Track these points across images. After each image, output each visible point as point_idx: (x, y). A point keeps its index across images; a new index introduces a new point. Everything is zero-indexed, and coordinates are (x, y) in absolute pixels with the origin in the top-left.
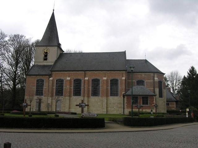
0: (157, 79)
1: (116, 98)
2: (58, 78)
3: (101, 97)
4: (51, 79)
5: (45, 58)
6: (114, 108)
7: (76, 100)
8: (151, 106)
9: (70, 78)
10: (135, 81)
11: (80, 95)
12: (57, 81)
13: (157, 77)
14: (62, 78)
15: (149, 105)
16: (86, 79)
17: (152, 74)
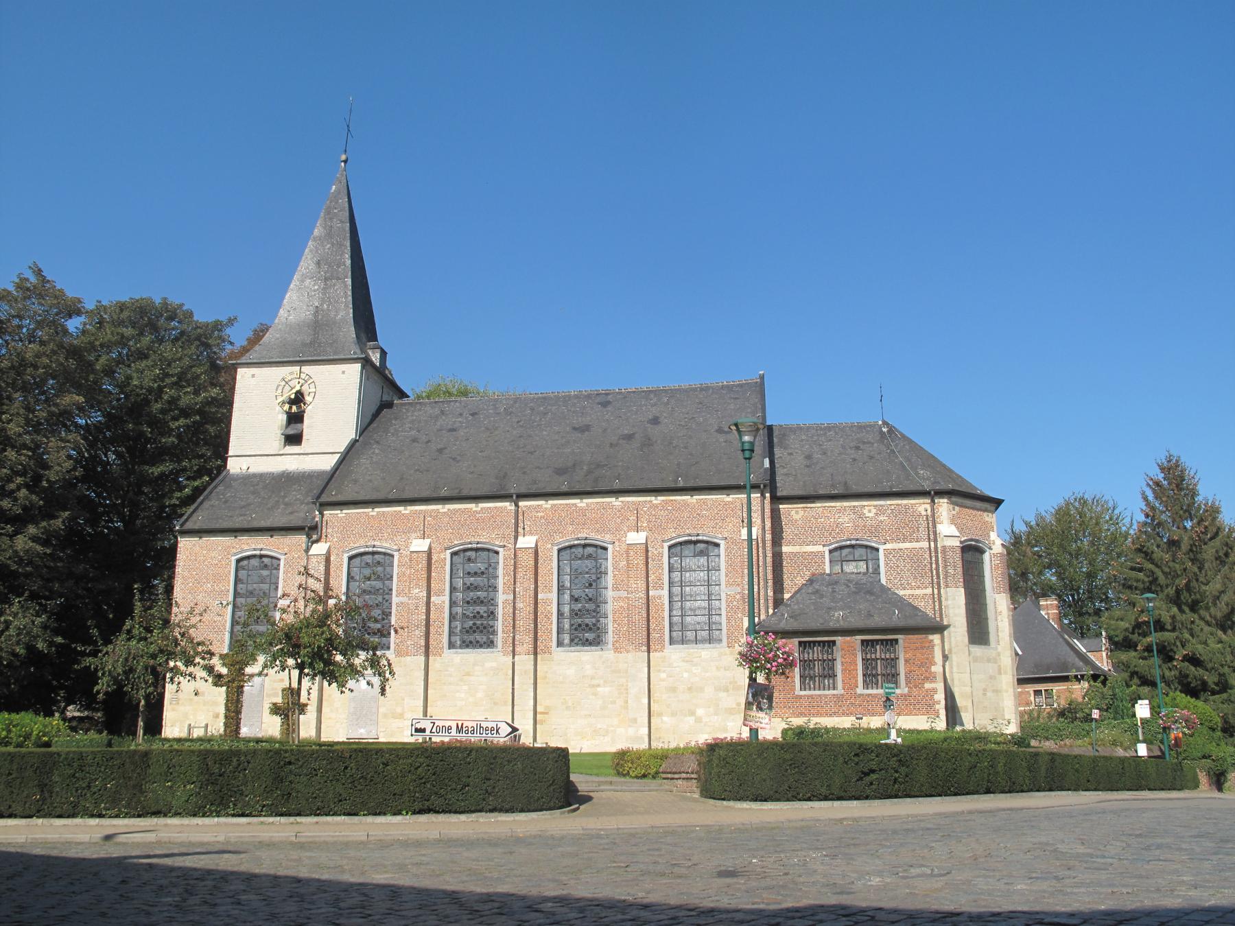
0: (953, 530)
1: (705, 652)
2: (359, 546)
3: (616, 650)
4: (319, 549)
5: (291, 431)
6: (692, 713)
7: (468, 674)
8: (915, 692)
9: (428, 541)
10: (820, 548)
11: (490, 644)
12: (357, 561)
13: (953, 521)
14: (384, 545)
15: (906, 690)
16: (527, 542)
17: (922, 506)
